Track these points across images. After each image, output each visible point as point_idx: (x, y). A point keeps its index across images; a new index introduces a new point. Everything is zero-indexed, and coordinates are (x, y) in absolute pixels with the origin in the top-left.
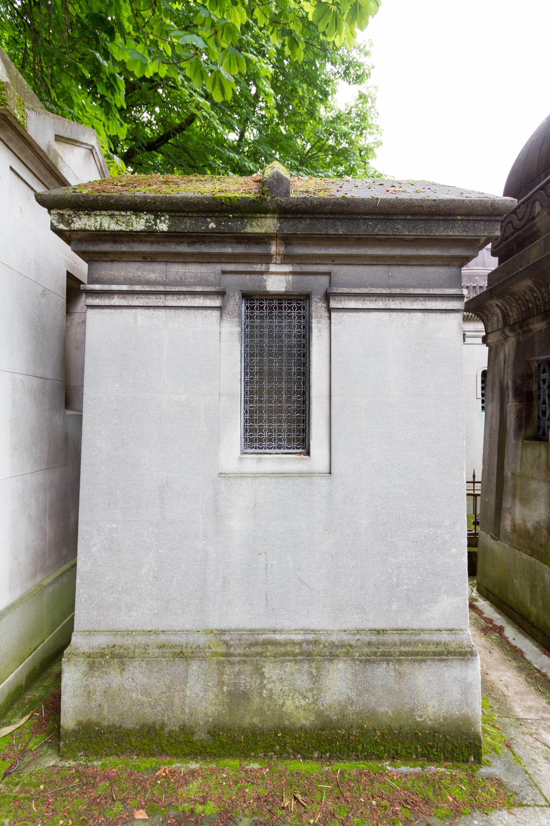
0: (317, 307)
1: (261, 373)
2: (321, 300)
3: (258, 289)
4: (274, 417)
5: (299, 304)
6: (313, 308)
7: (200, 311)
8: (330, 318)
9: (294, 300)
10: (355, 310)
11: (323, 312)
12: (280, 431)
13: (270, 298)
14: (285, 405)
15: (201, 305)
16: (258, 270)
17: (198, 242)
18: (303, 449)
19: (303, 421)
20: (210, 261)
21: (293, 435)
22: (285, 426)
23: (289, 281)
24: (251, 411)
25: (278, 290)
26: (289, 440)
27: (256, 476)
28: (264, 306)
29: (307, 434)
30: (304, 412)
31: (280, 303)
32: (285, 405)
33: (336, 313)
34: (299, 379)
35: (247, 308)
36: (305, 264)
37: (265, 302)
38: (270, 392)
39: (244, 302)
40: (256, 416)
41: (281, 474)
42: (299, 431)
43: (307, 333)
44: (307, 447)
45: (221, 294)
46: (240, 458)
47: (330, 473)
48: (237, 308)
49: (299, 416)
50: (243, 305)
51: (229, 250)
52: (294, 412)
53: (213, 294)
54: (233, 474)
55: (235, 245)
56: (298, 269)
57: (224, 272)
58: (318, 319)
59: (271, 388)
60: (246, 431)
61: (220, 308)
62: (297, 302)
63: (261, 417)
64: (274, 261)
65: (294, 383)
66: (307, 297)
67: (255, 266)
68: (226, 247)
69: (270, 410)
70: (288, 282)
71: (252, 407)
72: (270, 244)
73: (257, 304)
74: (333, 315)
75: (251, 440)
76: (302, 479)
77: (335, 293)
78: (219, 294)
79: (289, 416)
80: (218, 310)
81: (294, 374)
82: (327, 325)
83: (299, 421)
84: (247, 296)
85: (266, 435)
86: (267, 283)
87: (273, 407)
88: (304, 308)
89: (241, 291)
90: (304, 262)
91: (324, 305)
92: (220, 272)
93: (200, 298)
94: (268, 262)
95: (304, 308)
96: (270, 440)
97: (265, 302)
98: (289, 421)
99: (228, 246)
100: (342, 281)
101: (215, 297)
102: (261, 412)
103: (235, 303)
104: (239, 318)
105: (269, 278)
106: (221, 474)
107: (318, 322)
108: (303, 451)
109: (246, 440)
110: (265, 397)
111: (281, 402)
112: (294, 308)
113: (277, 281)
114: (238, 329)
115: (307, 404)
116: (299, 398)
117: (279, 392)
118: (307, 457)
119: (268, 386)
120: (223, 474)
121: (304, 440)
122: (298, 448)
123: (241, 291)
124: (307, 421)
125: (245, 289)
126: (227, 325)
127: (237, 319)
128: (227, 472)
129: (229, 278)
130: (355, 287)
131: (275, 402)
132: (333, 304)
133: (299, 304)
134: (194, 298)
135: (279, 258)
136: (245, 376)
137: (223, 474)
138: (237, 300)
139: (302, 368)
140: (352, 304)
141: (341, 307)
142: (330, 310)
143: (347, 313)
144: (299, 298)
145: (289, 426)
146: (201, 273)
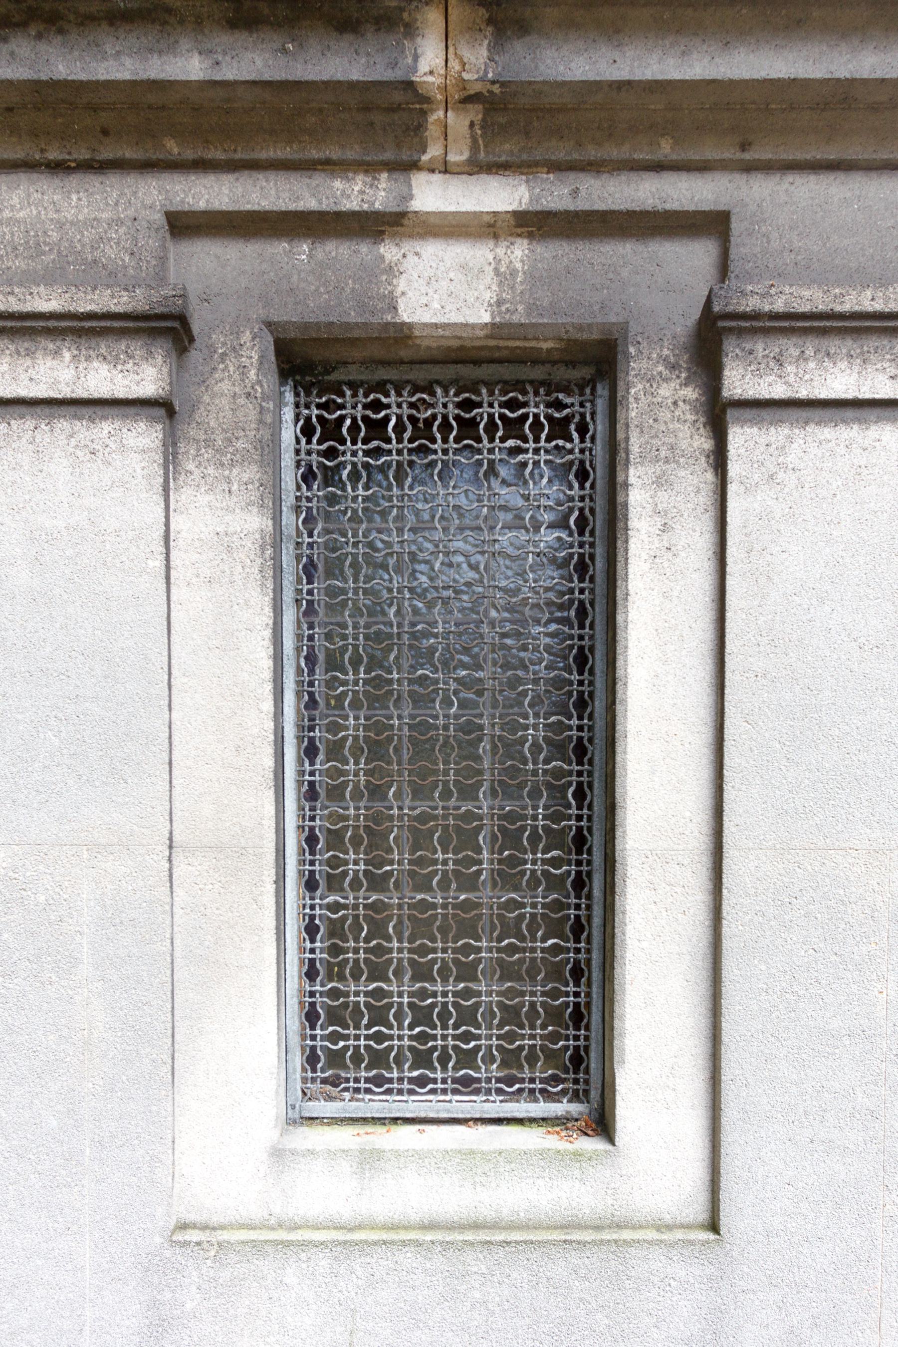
0: (656, 404)
1: (376, 747)
2: (673, 367)
3: (353, 317)
4: (442, 954)
5: (559, 405)
6: (634, 410)
7: (63, 425)
8: (719, 460)
9: (537, 384)
10: (849, 413)
11: (685, 431)
12: (468, 1016)
13: (419, 375)
14: (489, 897)
15: (65, 392)
16: (353, 204)
17: (23, 25)
18: (576, 1097)
19: (577, 973)
20: (106, 154)
21: (530, 1038)
22: (489, 992)
23: (513, 273)
24: (336, 930)
25: (455, 318)
26: (510, 1059)
27: (353, 1239)
28: (387, 419)
29: (595, 1034)
30: (578, 929)
31: (467, 405)
32: (489, 897)
33: (751, 431)
34: (558, 774)
35: (308, 431)
36: (594, 167)
37: (392, 399)
38: (419, 839)
39: (289, 397)
40: (356, 950)
41: (476, 1226)
42: (554, 1015)
43: (599, 551)
44: (594, 1094)
45: (168, 328)
46: (278, 1154)
47: (714, 1226)
48: (253, 414)
49: (556, 950)
50: (288, 414)
51: (188, 64)
52: (533, 928)
53: (123, 333)
54: (242, 1226)
55: (225, 39)
56: (557, 194)
57: (183, 225)
58: (659, 468)
59: (423, 818)
60: (311, 1017)
61: (163, 408)
62: (549, 391)
63: (379, 951)
64: (433, 152)
65: (535, 794)
66: (597, 362)
67: (338, 184)
68: (172, 49)
69: (421, 923)
70: (505, 277)
71: (335, 907)
72: (411, 30)
73: (353, 408)
74: (740, 437)
75: (336, 1059)
76: (575, 1258)
77: (756, 316)
78: (154, 333)
79: (512, 949)
80: (153, 419)
81: (536, 748)
82: (705, 498)
83: (555, 973)
84: (304, 361)
85: (402, 1036)
86: (401, 284)
87: (434, 906)
88: (583, 430)
89: (269, 325)
90: (592, 153)
91: (691, 393)
92: (158, 218)
93: (57, 353)
94: (405, 156)
95: (583, 430)
96: (422, 1059)
97: (392, 399)
98: (507, 972)
99: (185, 43)
100: (789, 258)
101: (136, 346)
102: (378, 929)
103: (238, 382)
104: (262, 464)
105: (412, 259)
106: (183, 1226)
107: (660, 482)
108: (575, 1108)
109: (312, 1059)
110: (399, 861)
111: (470, 883)
112: (537, 426)
113: (445, 288)
114: (256, 522)
115: (597, 893)
116: (555, 862)
117: (466, 838)
118: (593, 1144)
119: (412, 808)
120: (194, 1226)
121: (578, 1060)
122: (548, 1096)
123: (269, 325)
124: (596, 975)
125: (287, 313)
126: (204, 499)
127: (251, 473)
128: (215, 1220)
129: (209, 265)
130: (859, 278)
131: (444, 885)
132: (739, 381)
133: (559, 405)
134: (29, 353)
135: (459, 122)
136: (300, 762)
137: (194, 1226)
138: (252, 374)
139: (575, 722)
140: (839, 379)
141: (779, 391)
142: (718, 414)
143: (811, 428)
144: (562, 373)
145: (509, 993)
146: (60, 225)
